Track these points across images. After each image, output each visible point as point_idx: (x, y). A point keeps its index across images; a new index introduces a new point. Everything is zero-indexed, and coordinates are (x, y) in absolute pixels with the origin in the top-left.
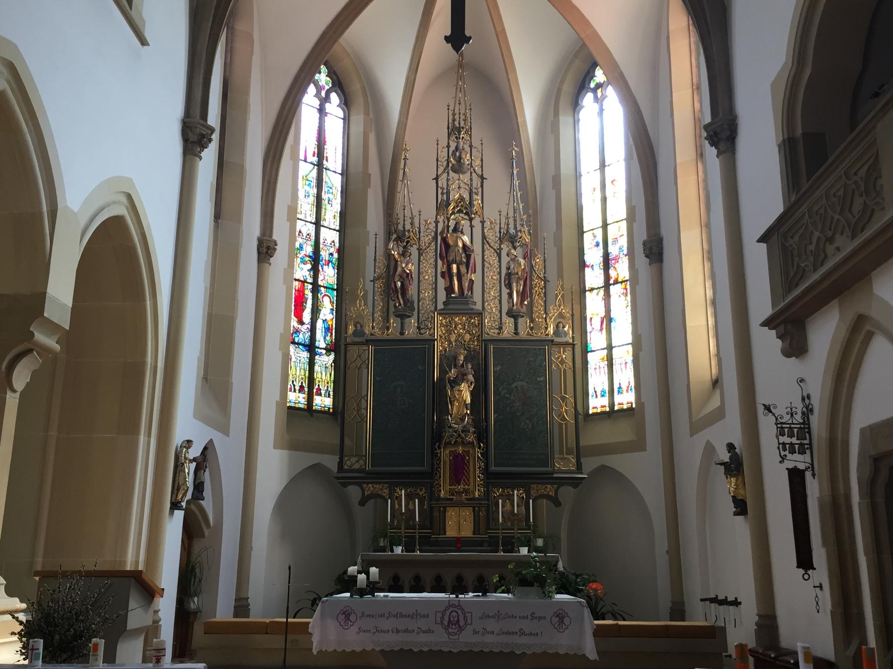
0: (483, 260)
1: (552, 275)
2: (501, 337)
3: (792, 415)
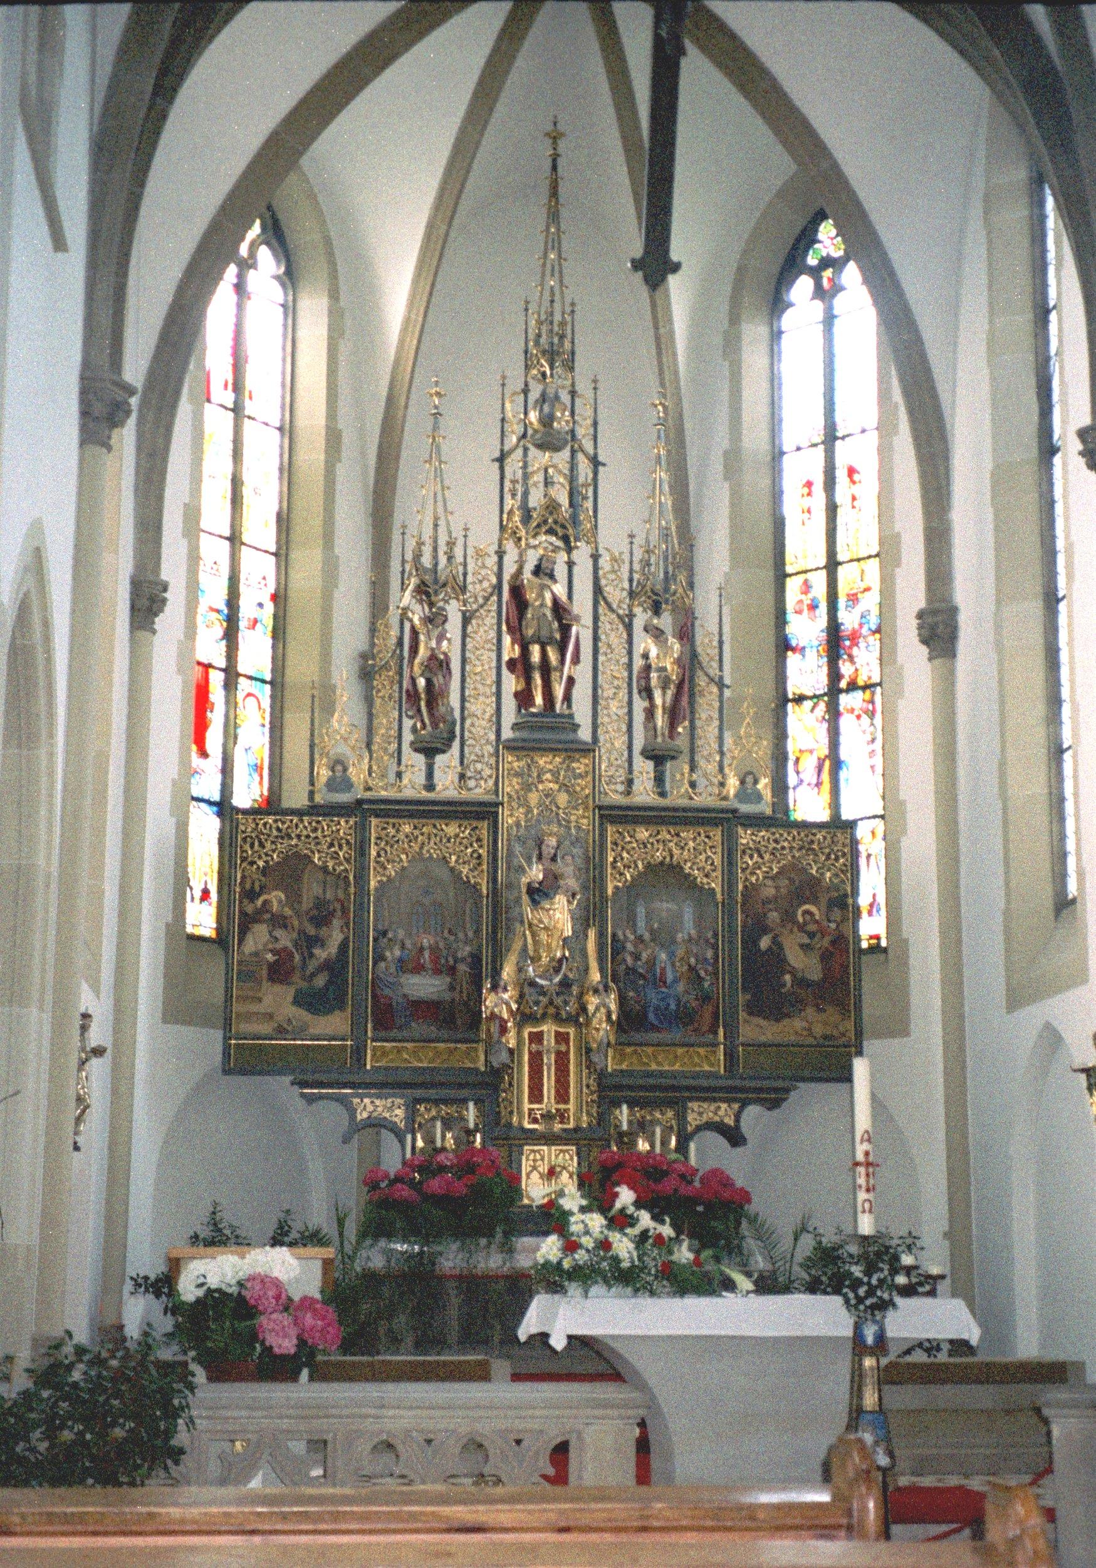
0: (596, 639)
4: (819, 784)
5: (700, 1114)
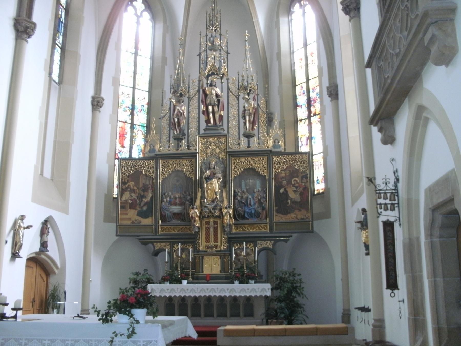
0: (228, 103)
3: (386, 184)
4: (307, 144)
5: (261, 245)
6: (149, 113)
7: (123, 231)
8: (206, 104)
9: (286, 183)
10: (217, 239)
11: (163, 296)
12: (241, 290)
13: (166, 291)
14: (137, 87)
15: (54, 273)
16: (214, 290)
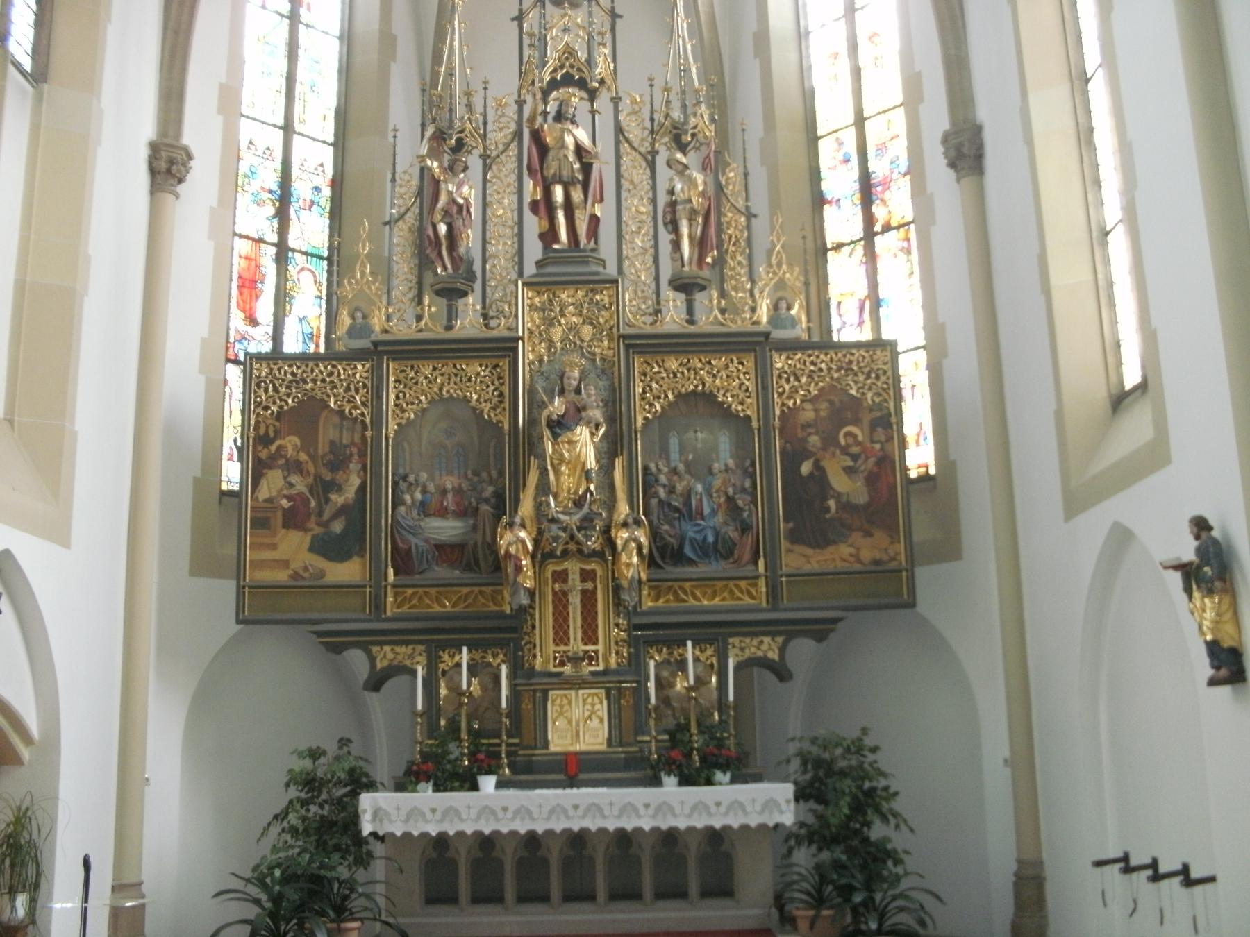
0: (619, 176)
1: (760, 203)
2: (659, 329)
4: (861, 323)
5: (742, 649)
6: (336, 214)
7: (260, 607)
8: (544, 179)
9: (819, 444)
10: (595, 631)
11: (416, 833)
12: (694, 808)
13: (429, 815)
14: (298, 127)
15: (18, 761)
16: (600, 810)
